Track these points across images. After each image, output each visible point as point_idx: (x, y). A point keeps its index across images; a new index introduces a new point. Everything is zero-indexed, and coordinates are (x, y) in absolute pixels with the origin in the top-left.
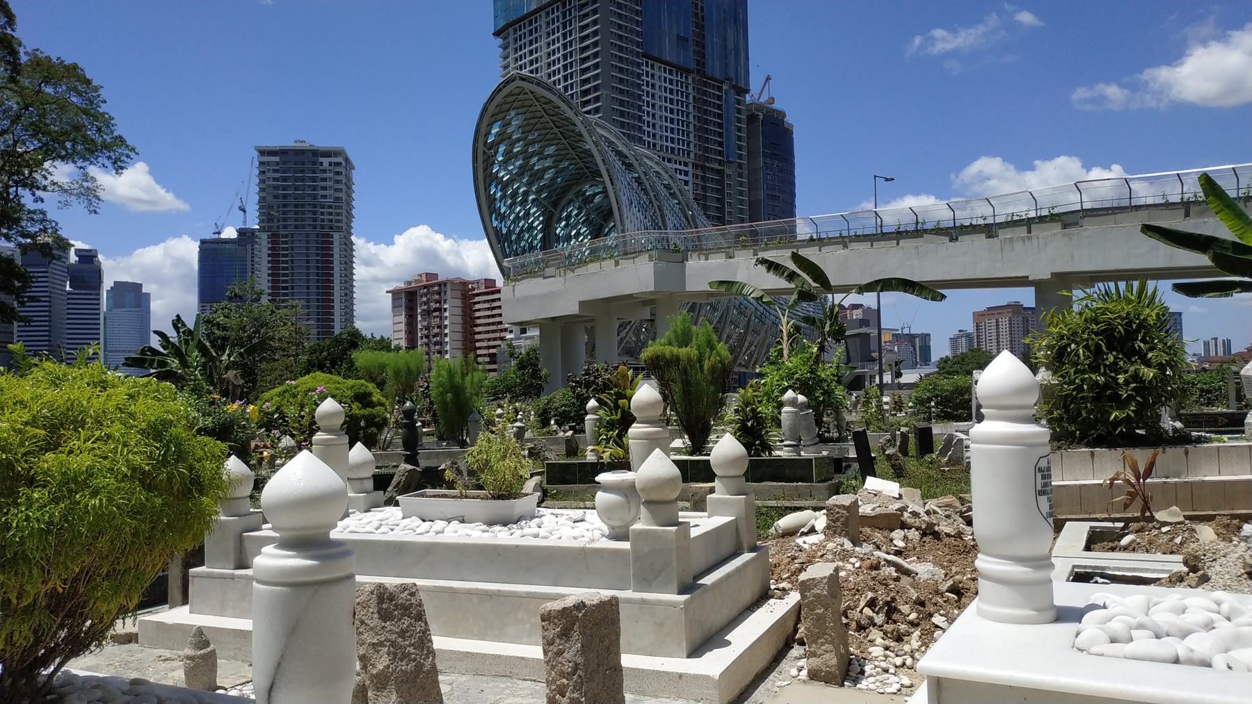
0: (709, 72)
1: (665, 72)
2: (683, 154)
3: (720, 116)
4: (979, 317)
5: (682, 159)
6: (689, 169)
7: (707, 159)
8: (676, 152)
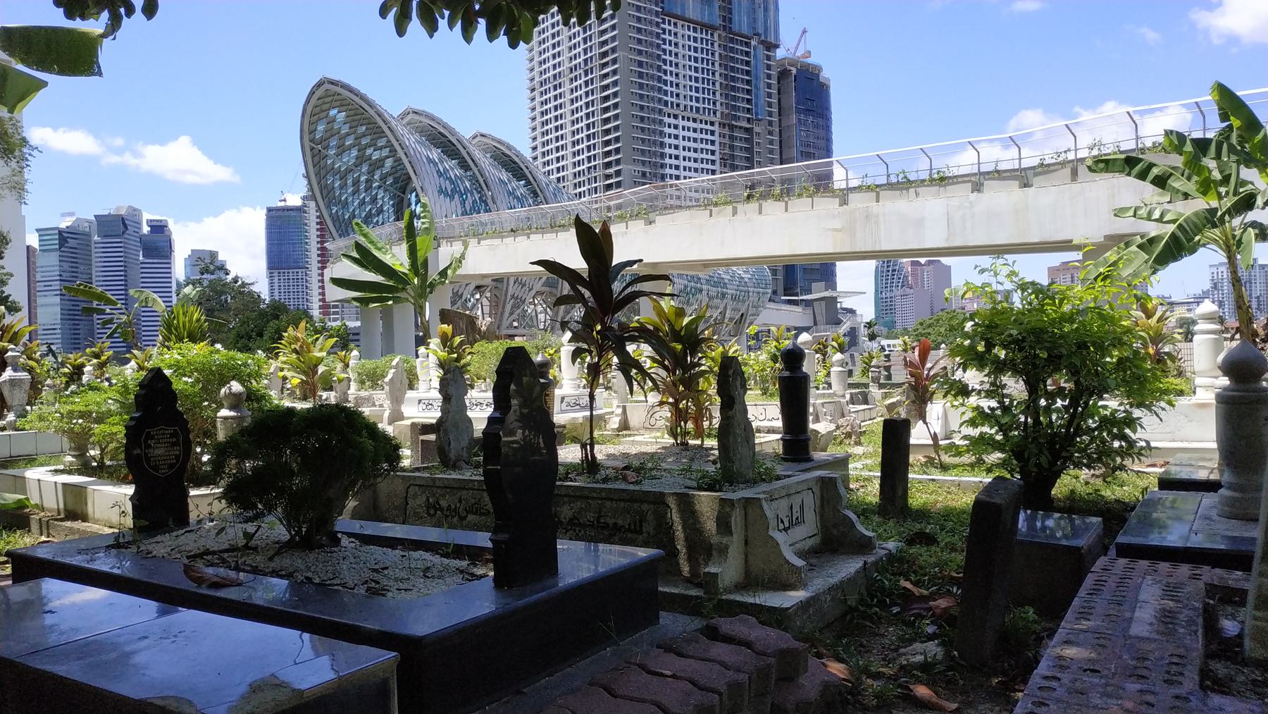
0: (735, 28)
1: (689, 30)
2: (709, 114)
3: (748, 73)
4: (1053, 271)
5: (708, 119)
6: (716, 128)
7: (737, 118)
8: (701, 112)
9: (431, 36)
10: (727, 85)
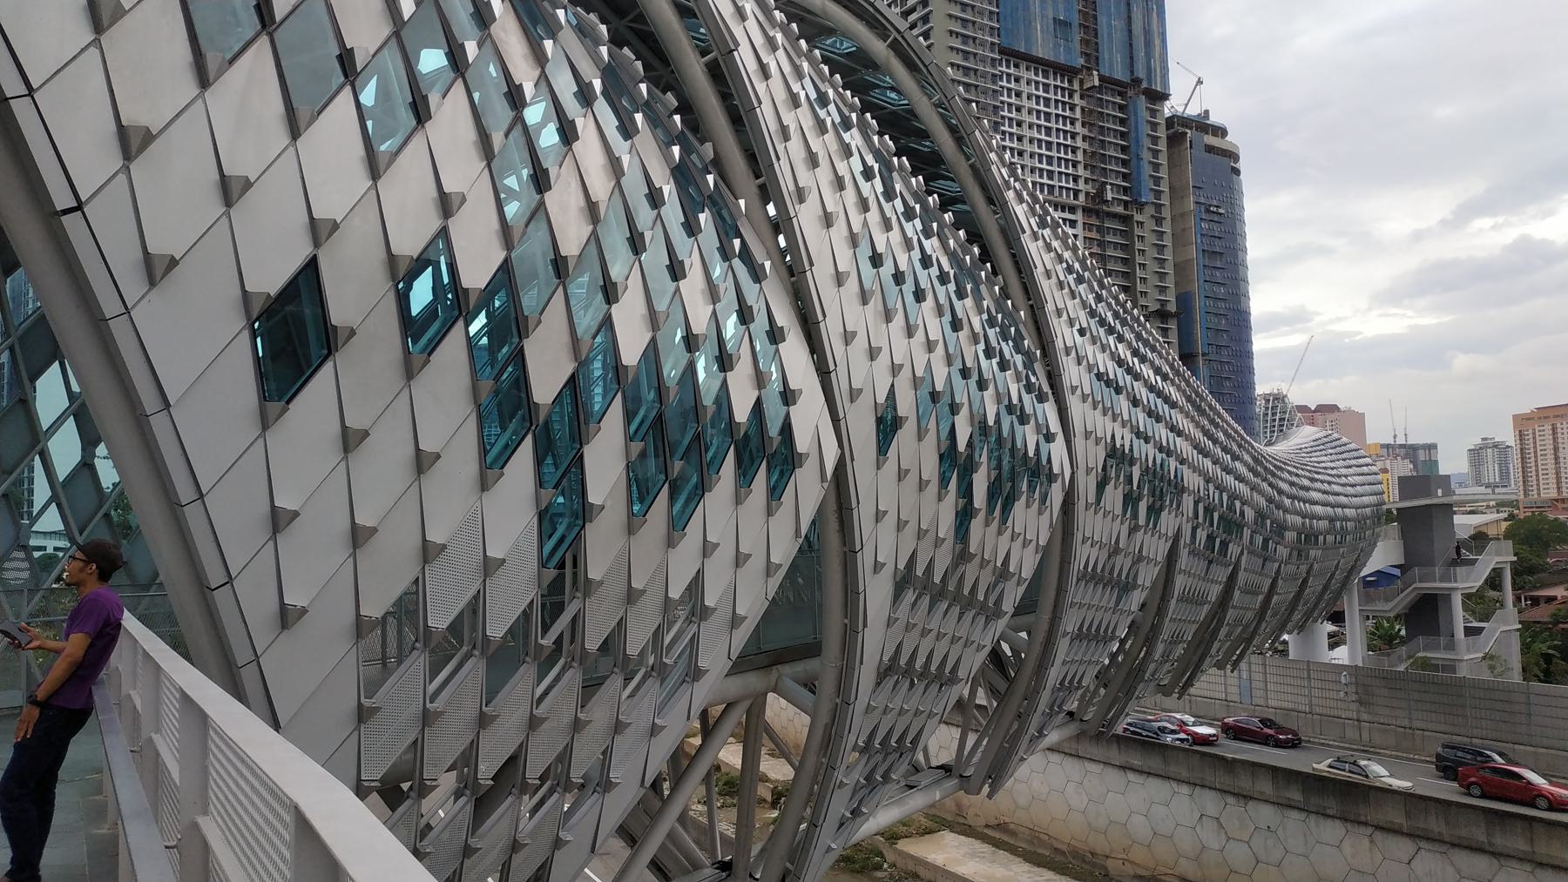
9: (907, 418)
10: (1093, 153)
